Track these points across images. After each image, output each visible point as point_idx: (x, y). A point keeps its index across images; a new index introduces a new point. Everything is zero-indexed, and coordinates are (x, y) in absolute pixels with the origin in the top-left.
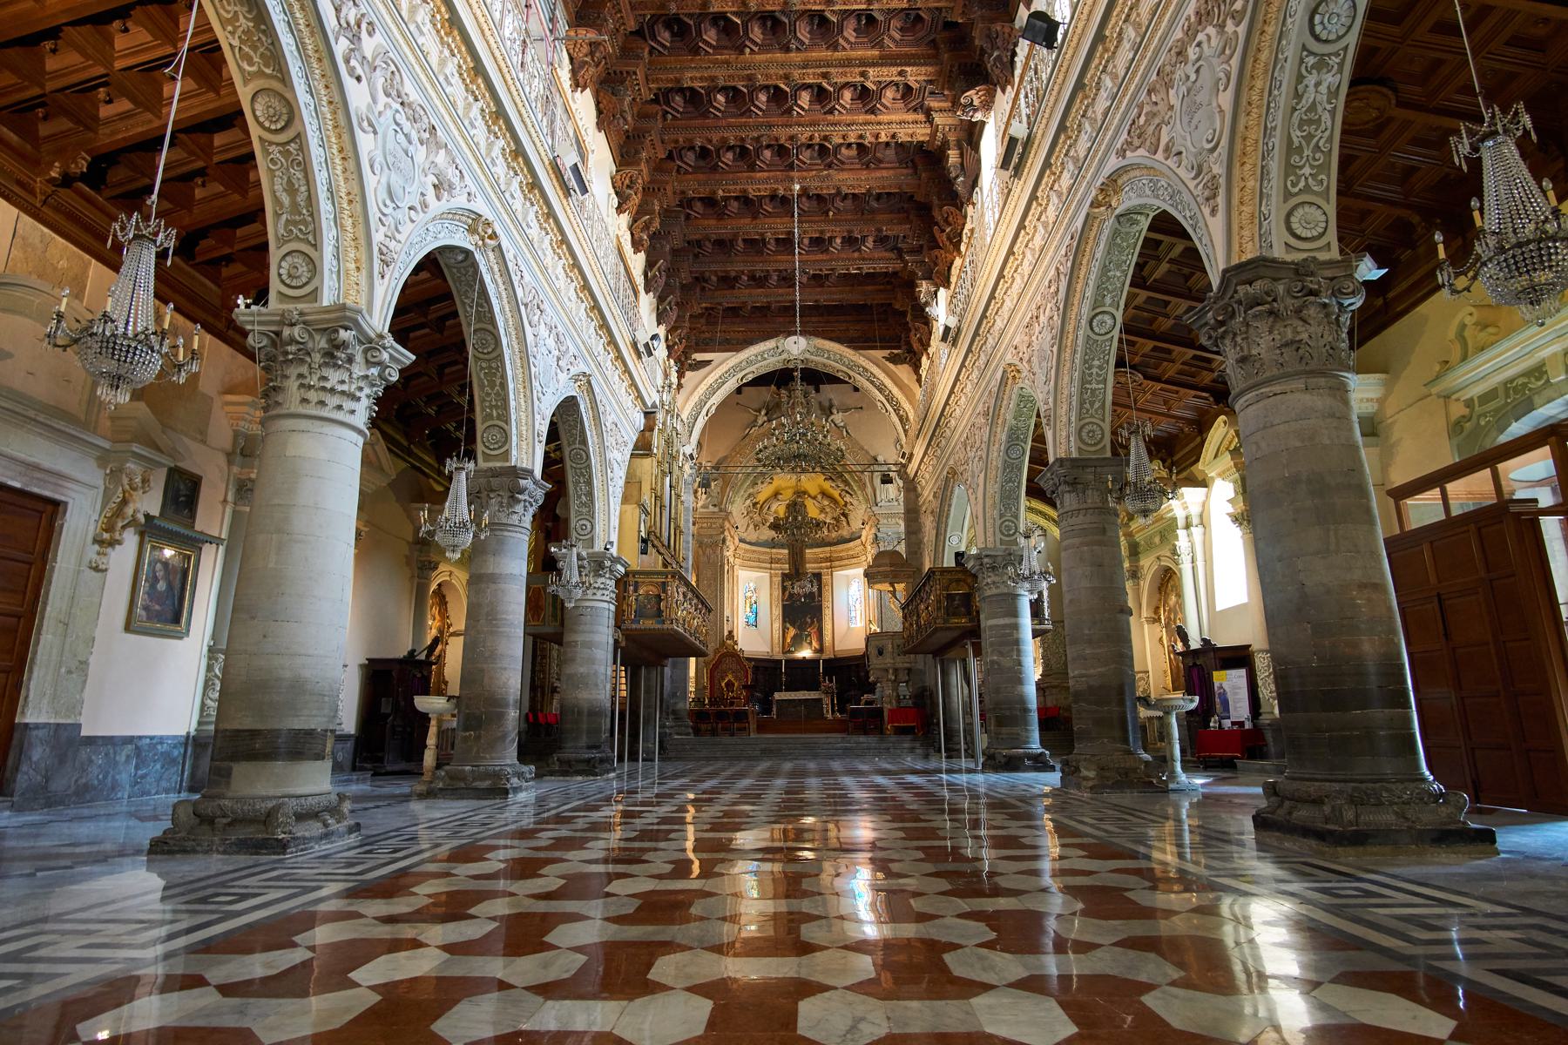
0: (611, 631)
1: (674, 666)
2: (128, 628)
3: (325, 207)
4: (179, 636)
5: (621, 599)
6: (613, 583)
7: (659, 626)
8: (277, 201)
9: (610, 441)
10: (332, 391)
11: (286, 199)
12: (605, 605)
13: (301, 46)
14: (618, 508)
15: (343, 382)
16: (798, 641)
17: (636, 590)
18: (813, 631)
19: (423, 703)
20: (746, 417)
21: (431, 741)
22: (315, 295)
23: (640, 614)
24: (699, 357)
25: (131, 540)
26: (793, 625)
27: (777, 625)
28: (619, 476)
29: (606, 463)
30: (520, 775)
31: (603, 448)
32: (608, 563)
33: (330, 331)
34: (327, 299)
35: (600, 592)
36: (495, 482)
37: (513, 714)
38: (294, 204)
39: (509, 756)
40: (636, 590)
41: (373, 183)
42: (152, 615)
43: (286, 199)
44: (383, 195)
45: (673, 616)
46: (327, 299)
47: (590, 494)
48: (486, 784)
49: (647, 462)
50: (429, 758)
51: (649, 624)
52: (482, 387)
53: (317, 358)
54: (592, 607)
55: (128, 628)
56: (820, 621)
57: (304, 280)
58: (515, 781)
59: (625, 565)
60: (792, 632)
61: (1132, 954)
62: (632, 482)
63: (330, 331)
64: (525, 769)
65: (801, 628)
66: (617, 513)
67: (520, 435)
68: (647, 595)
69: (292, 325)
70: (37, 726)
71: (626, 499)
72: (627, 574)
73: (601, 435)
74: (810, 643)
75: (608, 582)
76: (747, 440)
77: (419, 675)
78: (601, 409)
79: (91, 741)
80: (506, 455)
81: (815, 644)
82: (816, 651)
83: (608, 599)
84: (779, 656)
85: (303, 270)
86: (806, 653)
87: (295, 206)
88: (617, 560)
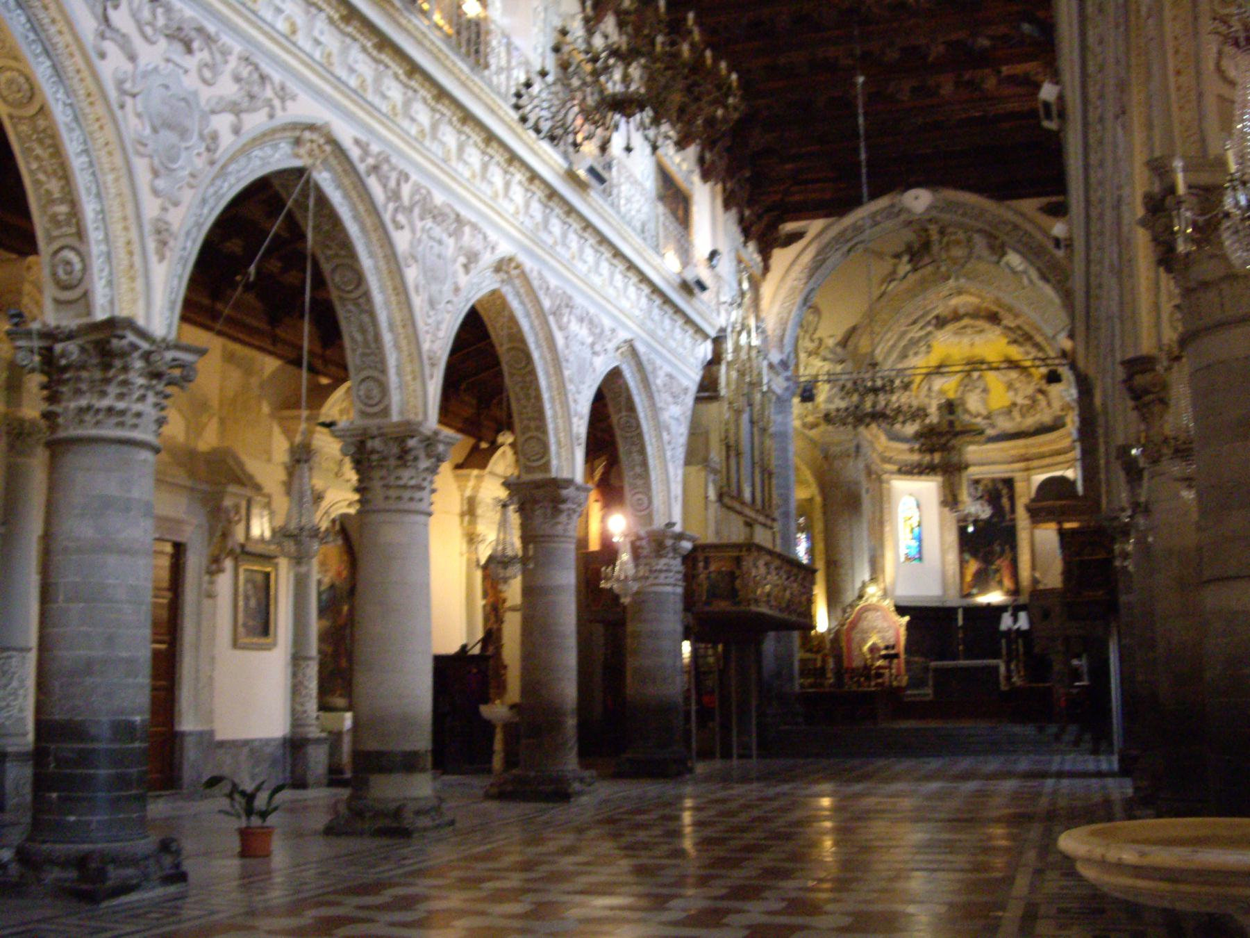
0: (680, 616)
1: (778, 640)
2: (235, 644)
3: (387, 338)
4: (268, 648)
5: (689, 577)
6: (679, 561)
7: (734, 608)
8: (353, 339)
9: (662, 398)
10: (405, 487)
11: (359, 337)
12: (669, 589)
13: (363, 228)
14: (680, 472)
15: (412, 478)
16: (982, 580)
17: (706, 567)
18: (1002, 563)
19: (487, 711)
20: (886, 266)
21: (498, 745)
22: (386, 412)
23: (713, 594)
24: (790, 227)
25: (228, 564)
26: (974, 555)
27: (953, 557)
28: (678, 434)
29: (659, 427)
30: (582, 780)
31: (655, 410)
32: (669, 542)
33: (401, 440)
34: (395, 417)
35: (663, 575)
36: (539, 493)
37: (571, 722)
38: (366, 342)
39: (571, 762)
40: (706, 567)
41: (418, 301)
42: (250, 632)
43: (359, 337)
44: (426, 307)
45: (751, 596)
46: (395, 417)
47: (644, 464)
48: (550, 788)
49: (713, 408)
50: (497, 762)
51: (723, 605)
52: (518, 400)
53: (393, 462)
54: (656, 593)
55: (235, 644)
56: (1014, 547)
57: (376, 400)
58: (576, 786)
59: (690, 539)
60: (973, 566)
61: (385, 841)
62: (697, 432)
63: (401, 440)
64: (587, 774)
65: (987, 559)
66: (680, 478)
67: (558, 443)
68: (719, 572)
69: (373, 437)
70: (191, 734)
71: (688, 462)
72: (695, 548)
73: (651, 397)
74: (1000, 583)
75: (672, 562)
76: (884, 300)
77: (475, 671)
78: (649, 368)
79: (221, 744)
80: (546, 467)
81: (1008, 583)
82: (1008, 593)
83: (672, 581)
84: (953, 600)
85: (376, 392)
86: (994, 597)
87: (366, 342)
88: (680, 537)
